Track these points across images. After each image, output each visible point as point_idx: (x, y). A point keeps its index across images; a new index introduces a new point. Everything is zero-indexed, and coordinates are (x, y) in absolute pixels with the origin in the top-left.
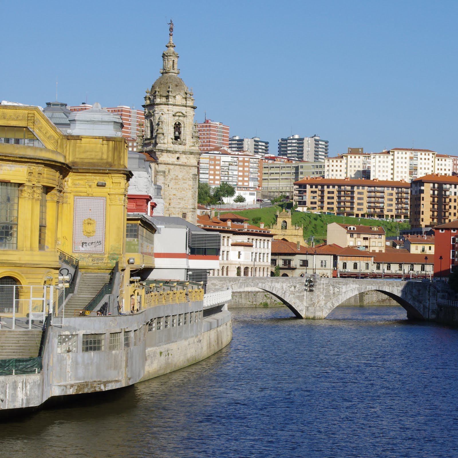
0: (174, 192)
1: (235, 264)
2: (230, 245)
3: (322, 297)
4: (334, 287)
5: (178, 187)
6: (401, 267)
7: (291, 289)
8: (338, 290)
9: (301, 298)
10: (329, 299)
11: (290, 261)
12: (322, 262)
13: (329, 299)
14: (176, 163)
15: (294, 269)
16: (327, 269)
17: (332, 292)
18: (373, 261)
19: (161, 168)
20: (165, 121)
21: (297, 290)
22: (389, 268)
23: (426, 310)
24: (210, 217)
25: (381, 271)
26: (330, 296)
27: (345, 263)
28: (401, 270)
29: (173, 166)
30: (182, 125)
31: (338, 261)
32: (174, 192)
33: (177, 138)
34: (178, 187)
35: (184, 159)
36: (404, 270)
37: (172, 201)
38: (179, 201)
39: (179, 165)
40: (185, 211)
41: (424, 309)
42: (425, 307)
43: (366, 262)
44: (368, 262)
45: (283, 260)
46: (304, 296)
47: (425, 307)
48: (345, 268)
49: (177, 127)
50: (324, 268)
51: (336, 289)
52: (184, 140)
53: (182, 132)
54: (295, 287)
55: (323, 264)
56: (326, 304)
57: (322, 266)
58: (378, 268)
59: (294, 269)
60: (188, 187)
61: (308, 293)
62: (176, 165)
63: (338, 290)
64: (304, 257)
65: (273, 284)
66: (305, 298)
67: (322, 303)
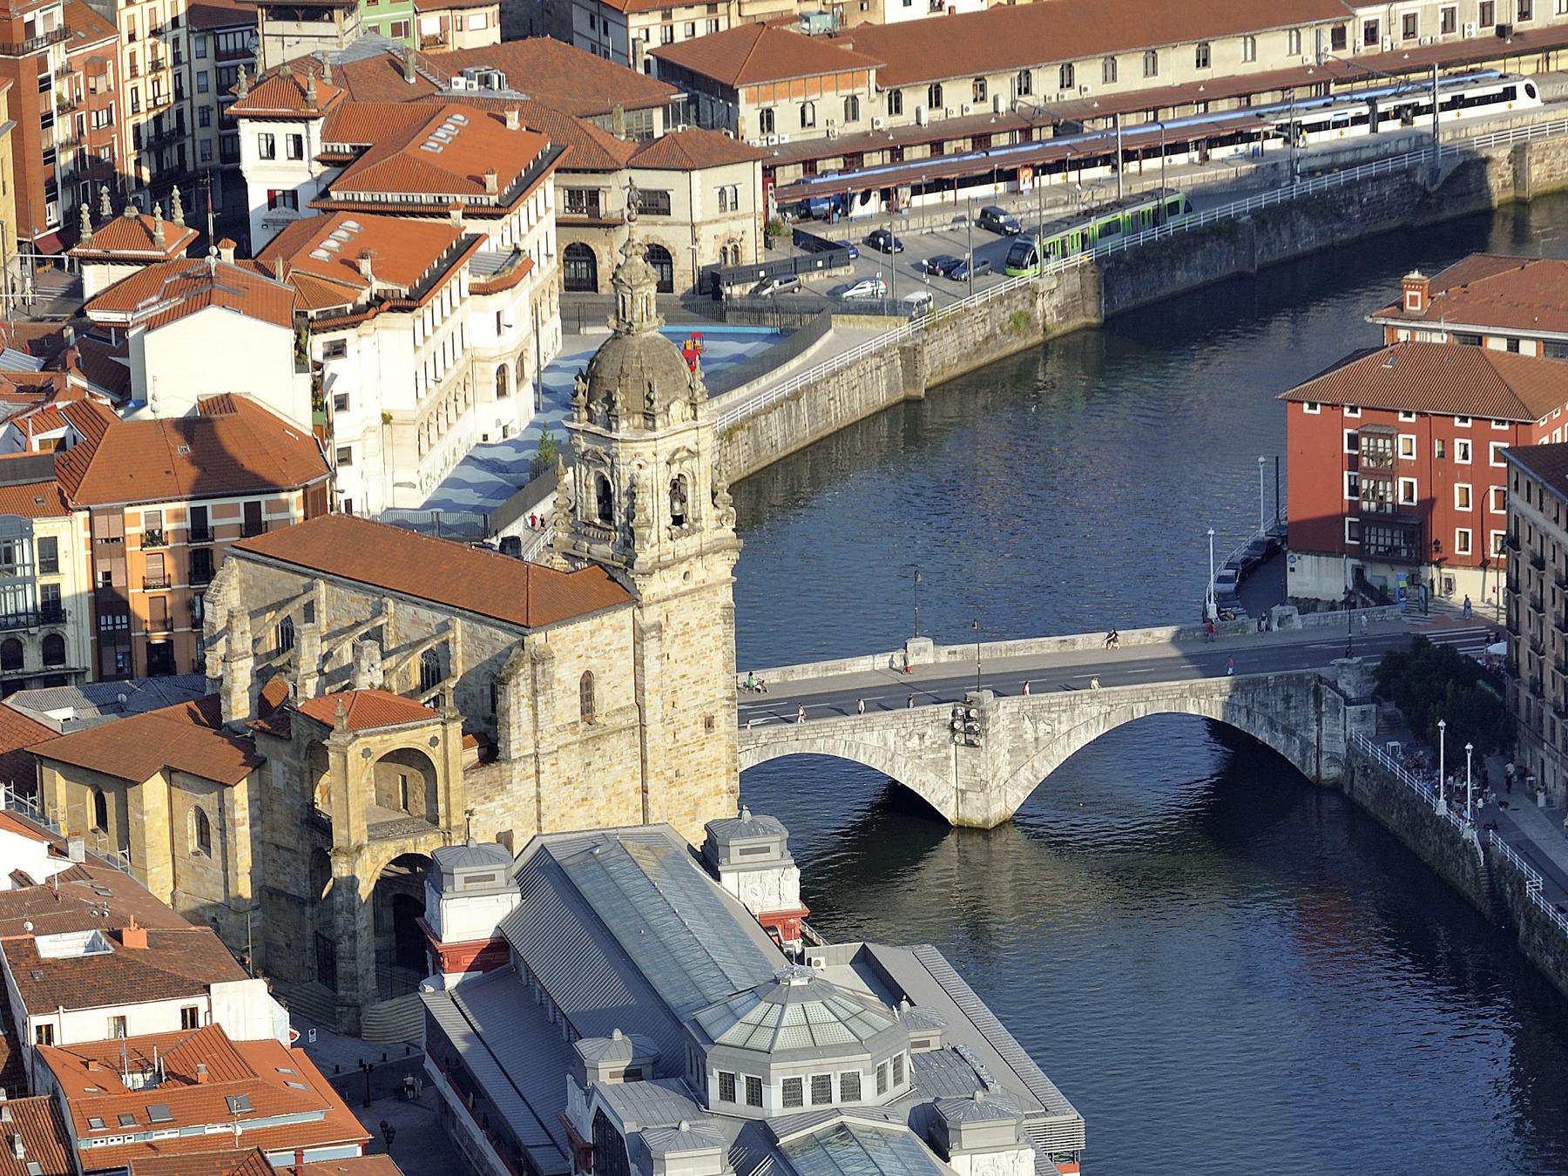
0: (683, 668)
1: (490, 360)
2: (465, 293)
3: (1003, 758)
4: (1034, 719)
5: (690, 651)
6: (982, 88)
7: (909, 744)
8: (1049, 729)
9: (940, 767)
10: (1022, 758)
11: (594, 195)
12: (722, 192)
13: (1022, 758)
14: (682, 589)
15: (611, 226)
16: (744, 216)
17: (1030, 736)
18: (873, 86)
19: (651, 616)
20: (649, 483)
21: (928, 743)
22: (936, 100)
23: (1311, 753)
24: (304, 94)
25: (906, 118)
26: (1025, 749)
27: (769, 111)
28: (982, 99)
29: (675, 602)
30: (689, 480)
31: (741, 107)
32: (683, 668)
33: (678, 520)
34: (690, 651)
35: (699, 573)
36: (995, 100)
37: (679, 693)
38: (695, 688)
39: (691, 592)
40: (709, 710)
41: (1303, 753)
42: (1306, 746)
43: (849, 92)
44: (856, 91)
45: (565, 188)
46: (948, 758)
47: (1306, 746)
48: (770, 128)
49: (677, 489)
50: (729, 213)
51: (1042, 726)
52: (695, 520)
53: (689, 499)
54: (922, 737)
55: (727, 200)
56: (1014, 774)
57: (723, 207)
58: (895, 107)
59: (611, 226)
60: (712, 644)
61: (961, 751)
62: (684, 594)
63: (1049, 729)
64: (649, 180)
65: (857, 738)
66: (952, 763)
67: (1005, 772)
